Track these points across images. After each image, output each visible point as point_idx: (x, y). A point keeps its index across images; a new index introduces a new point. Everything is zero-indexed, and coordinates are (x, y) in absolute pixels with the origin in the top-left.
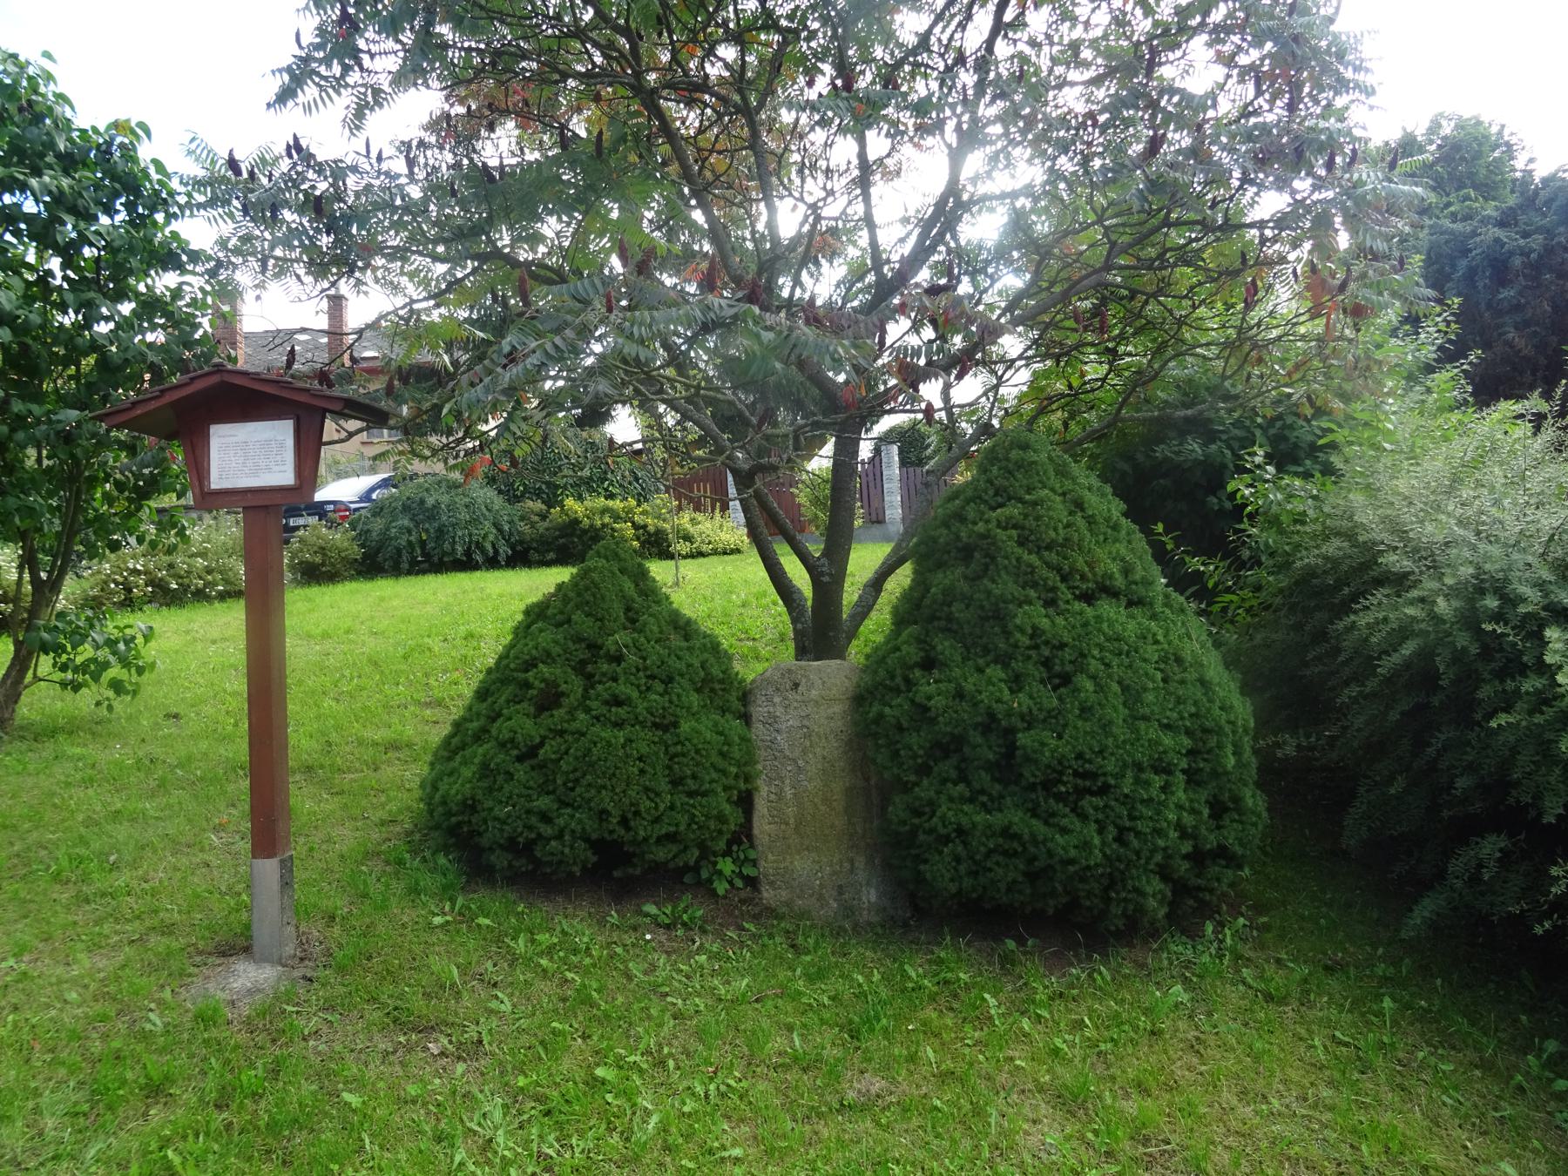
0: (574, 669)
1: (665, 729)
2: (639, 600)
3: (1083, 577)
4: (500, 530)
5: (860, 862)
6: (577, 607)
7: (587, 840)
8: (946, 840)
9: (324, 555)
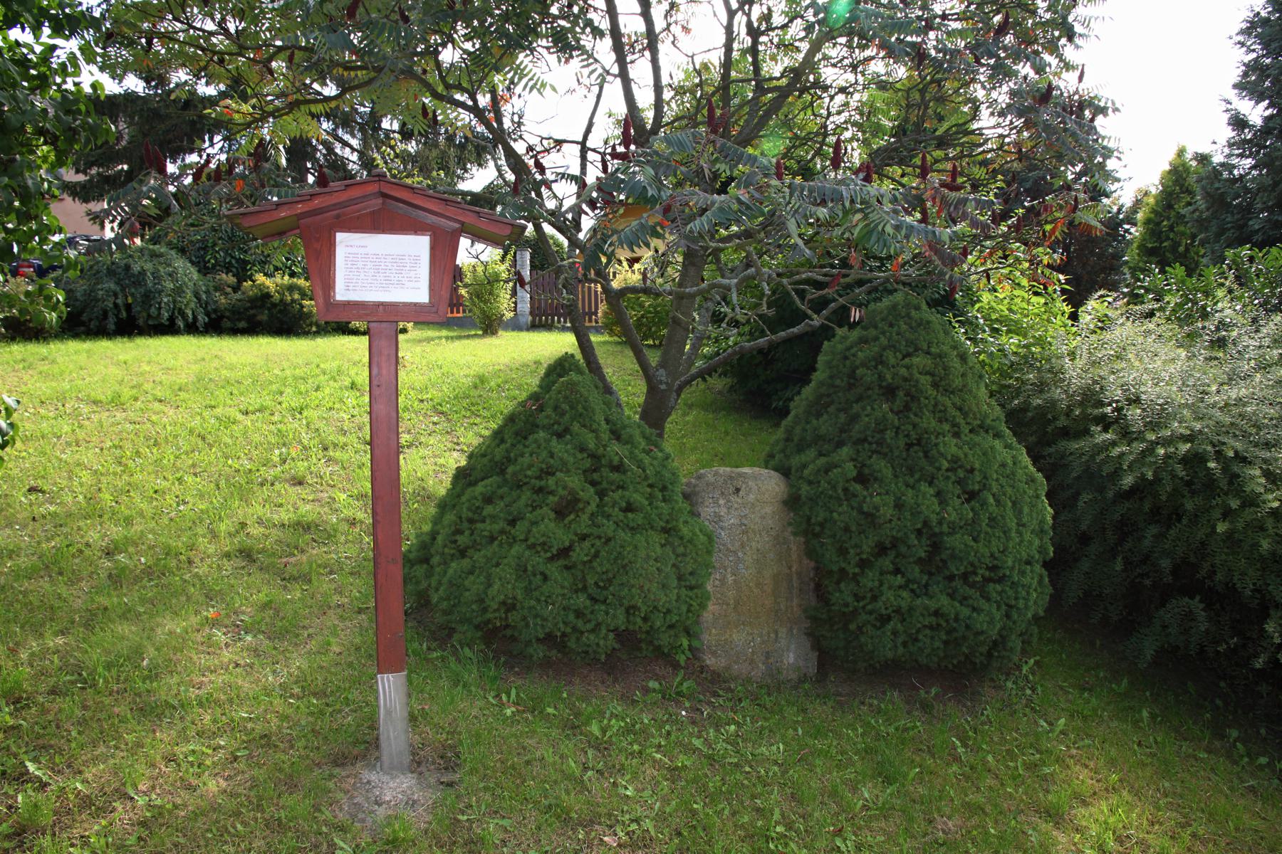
4: (199, 299)
5: (783, 632)
8: (885, 619)
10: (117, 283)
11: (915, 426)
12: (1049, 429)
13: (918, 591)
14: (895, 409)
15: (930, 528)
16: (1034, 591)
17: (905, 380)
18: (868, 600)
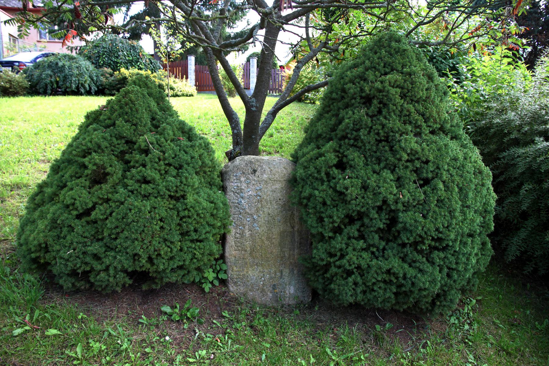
0: (117, 156)
1: (177, 199)
2: (159, 113)
3: (435, 122)
5: (286, 272)
6: (120, 116)
7: (125, 271)
8: (349, 273)
9: (11, 84)
10: (52, 71)
11: (383, 126)
12: (505, 140)
13: (377, 253)
14: (370, 114)
15: (389, 205)
16: (475, 256)
17: (380, 91)
18: (337, 258)
